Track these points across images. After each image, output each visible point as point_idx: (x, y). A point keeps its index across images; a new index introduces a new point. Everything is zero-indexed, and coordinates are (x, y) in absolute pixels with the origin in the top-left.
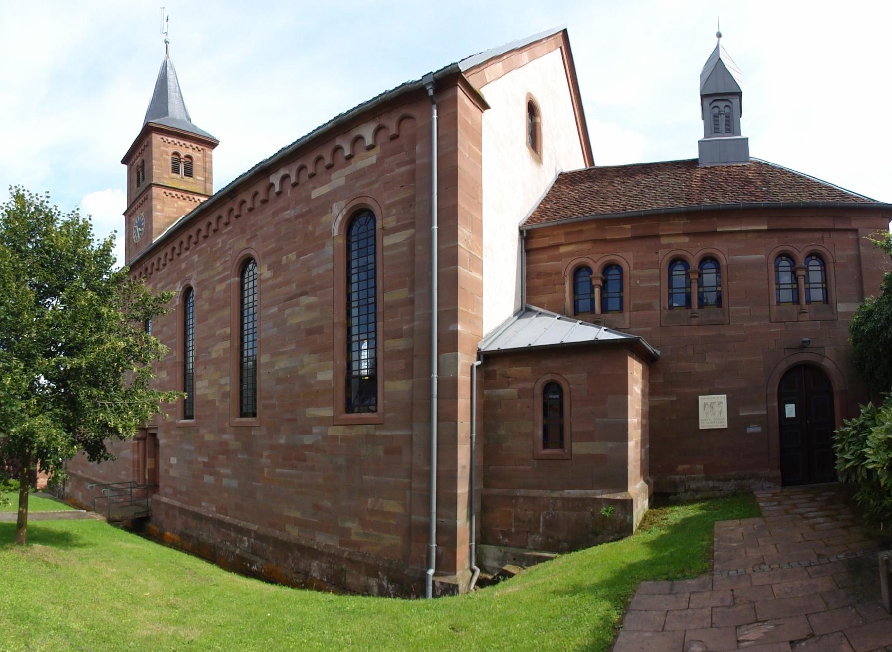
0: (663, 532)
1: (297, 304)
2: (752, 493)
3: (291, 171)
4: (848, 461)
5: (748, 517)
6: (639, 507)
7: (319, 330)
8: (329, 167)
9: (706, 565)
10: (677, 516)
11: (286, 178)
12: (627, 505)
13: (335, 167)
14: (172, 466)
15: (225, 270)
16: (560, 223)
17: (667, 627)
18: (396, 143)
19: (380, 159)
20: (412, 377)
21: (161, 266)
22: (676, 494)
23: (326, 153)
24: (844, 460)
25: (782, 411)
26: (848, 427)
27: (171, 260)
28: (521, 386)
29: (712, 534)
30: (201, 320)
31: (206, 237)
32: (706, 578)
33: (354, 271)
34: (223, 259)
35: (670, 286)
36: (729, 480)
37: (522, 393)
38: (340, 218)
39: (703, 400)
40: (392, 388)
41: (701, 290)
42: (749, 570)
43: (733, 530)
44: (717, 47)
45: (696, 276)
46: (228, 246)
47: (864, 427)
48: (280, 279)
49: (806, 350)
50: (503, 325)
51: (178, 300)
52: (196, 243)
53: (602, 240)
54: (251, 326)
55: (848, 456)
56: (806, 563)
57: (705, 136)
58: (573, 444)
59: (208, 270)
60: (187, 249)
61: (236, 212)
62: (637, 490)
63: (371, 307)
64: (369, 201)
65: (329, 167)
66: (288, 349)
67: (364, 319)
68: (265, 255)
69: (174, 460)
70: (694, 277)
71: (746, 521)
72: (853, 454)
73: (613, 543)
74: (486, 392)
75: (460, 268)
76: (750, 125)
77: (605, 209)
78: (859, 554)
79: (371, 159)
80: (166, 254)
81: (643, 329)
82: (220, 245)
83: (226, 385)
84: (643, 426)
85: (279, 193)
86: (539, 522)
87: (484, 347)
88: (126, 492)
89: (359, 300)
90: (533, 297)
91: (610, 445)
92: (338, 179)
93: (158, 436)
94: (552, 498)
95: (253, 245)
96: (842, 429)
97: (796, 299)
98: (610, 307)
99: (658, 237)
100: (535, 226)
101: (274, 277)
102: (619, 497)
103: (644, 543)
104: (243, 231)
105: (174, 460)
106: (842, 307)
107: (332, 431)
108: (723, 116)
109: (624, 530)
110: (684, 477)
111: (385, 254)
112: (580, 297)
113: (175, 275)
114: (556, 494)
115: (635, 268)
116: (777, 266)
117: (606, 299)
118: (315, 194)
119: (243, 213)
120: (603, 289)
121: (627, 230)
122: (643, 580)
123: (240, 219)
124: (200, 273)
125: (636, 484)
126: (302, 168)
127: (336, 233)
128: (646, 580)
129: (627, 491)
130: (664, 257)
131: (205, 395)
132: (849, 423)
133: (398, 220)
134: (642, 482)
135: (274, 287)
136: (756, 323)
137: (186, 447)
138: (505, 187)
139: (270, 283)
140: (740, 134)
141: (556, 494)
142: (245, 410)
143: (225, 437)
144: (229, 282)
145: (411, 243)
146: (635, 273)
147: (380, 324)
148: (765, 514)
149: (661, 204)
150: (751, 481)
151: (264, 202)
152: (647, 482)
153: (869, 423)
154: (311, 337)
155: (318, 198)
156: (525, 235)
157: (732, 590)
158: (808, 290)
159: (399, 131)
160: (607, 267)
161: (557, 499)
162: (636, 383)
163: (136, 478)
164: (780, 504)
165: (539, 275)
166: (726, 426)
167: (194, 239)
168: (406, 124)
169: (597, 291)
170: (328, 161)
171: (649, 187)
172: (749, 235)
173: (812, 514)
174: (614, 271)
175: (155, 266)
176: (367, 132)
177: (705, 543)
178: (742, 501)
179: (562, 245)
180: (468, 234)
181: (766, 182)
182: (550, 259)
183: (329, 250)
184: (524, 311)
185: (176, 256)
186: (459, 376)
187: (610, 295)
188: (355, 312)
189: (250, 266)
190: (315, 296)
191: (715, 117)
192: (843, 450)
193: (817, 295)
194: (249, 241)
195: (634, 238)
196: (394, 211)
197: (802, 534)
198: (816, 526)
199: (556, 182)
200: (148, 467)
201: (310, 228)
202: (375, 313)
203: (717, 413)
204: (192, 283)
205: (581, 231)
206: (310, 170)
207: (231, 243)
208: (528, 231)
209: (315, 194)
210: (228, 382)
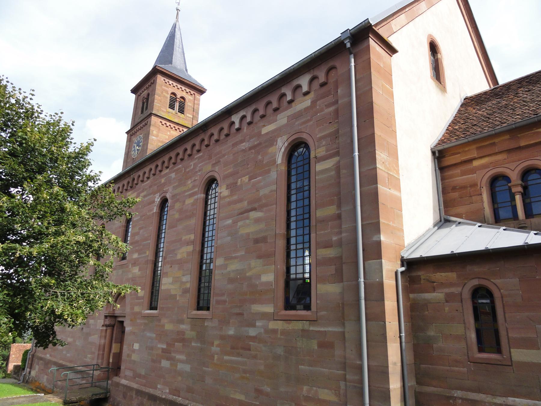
1: (248, 218)
3: (247, 112)
7: (264, 240)
8: (276, 110)
11: (244, 117)
13: (279, 110)
14: (134, 351)
15: (194, 187)
16: (470, 139)
18: (325, 88)
19: (314, 103)
20: (342, 282)
21: (145, 179)
23: (274, 99)
27: (154, 175)
28: (447, 290)
30: (172, 227)
31: (182, 160)
33: (293, 192)
34: (193, 179)
37: (449, 298)
38: (283, 150)
40: (325, 291)
46: (198, 169)
48: (235, 197)
50: (424, 235)
51: (155, 208)
52: (174, 164)
54: (210, 234)
59: (180, 186)
60: (167, 168)
61: (206, 142)
63: (306, 221)
64: (304, 136)
65: (276, 110)
66: (239, 254)
67: (300, 232)
68: (226, 177)
69: (136, 346)
74: (411, 296)
75: (379, 186)
77: (515, 119)
79: (307, 102)
80: (151, 170)
82: (192, 167)
83: (187, 282)
85: (238, 130)
87: (407, 255)
88: (89, 374)
89: (296, 216)
90: (451, 206)
92: (282, 119)
93: (125, 324)
95: (217, 169)
100: (446, 146)
101: (231, 195)
104: (210, 158)
105: (136, 346)
107: (272, 325)
111: (317, 178)
112: (500, 205)
113: (155, 187)
118: (264, 131)
119: (211, 144)
123: (209, 148)
124: (175, 188)
126: (256, 110)
127: (279, 161)
131: (169, 290)
133: (327, 150)
135: (230, 203)
137: (148, 334)
138: (415, 115)
139: (228, 200)
142: (201, 305)
143: (183, 327)
144: (196, 197)
145: (338, 168)
147: (313, 235)
151: (227, 135)
154: (257, 245)
155: (267, 134)
156: (437, 155)
159: (327, 79)
163: (100, 361)
165: (454, 189)
167: (173, 160)
168: (333, 73)
169: (518, 199)
170: (275, 105)
175: (141, 179)
176: (304, 81)
179: (475, 159)
180: (385, 157)
182: (464, 173)
183: (273, 175)
184: (443, 222)
185: (158, 172)
186: (384, 280)
188: (293, 225)
189: (214, 186)
190: (261, 211)
194: (214, 165)
196: (324, 143)
199: (462, 106)
200: (113, 351)
201: (260, 157)
202: (309, 226)
204: (168, 196)
205: (494, 144)
206: (261, 112)
207: (200, 167)
208: (440, 151)
209: (264, 131)
210: (189, 280)
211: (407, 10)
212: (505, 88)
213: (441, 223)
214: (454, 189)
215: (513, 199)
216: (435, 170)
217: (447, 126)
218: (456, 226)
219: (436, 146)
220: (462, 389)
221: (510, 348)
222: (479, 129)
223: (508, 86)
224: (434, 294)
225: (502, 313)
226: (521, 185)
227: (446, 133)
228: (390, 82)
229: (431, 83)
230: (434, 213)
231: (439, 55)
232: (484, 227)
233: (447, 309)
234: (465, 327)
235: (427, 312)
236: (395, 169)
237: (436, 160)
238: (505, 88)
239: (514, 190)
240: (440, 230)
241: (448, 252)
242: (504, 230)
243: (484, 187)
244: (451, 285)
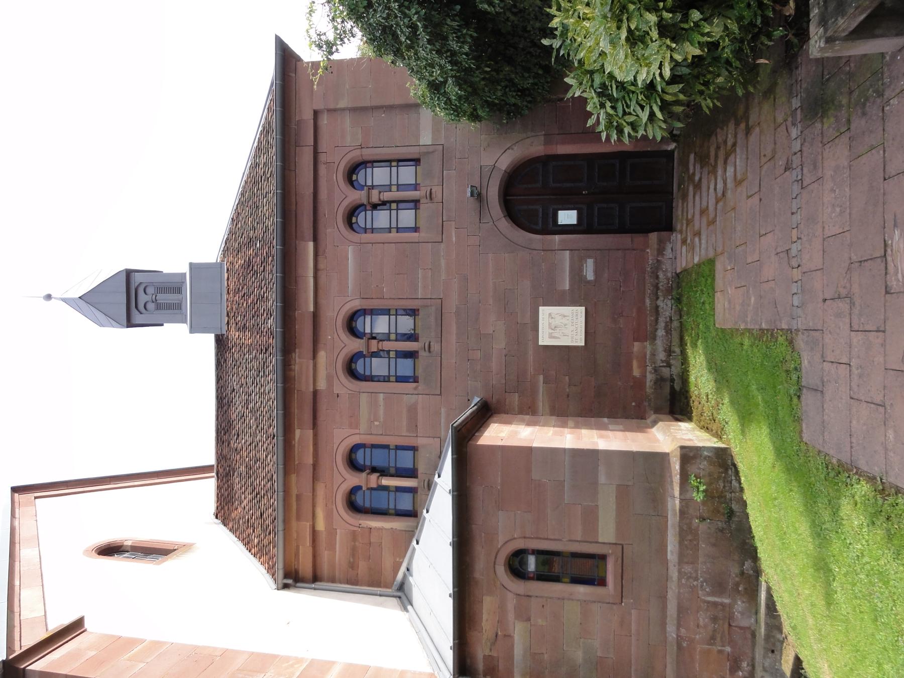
0: (726, 400)
2: (678, 275)
4: (652, 115)
5: (713, 279)
6: (690, 436)
9: (781, 339)
10: (704, 379)
12: (688, 455)
16: (281, 527)
17: (878, 399)
22: (672, 380)
24: (649, 126)
25: (567, 230)
26: (599, 115)
28: (511, 616)
29: (734, 332)
32: (801, 342)
35: (386, 379)
36: (657, 307)
37: (524, 615)
39: (544, 339)
41: (393, 337)
42: (796, 274)
43: (730, 302)
44: (65, 300)
45: (374, 342)
47: (603, 92)
49: (484, 192)
53: (314, 469)
55: (644, 116)
56: (796, 188)
57: (185, 322)
58: (600, 540)
62: (667, 437)
70: (374, 346)
71: (719, 283)
72: (642, 108)
73: (743, 479)
76: (172, 261)
77: (272, 462)
78: (796, 103)
81: (443, 420)
84: (577, 426)
86: (715, 604)
91: (602, 479)
94: (679, 579)
96: (602, 127)
97: (412, 205)
98: (410, 465)
99: (315, 393)
100: (280, 565)
102: (676, 466)
103: (743, 432)
106: (426, 139)
108: (159, 296)
109: (723, 461)
110: (649, 369)
114: (674, 573)
115: (357, 427)
116: (365, 230)
117: (397, 469)
120: (383, 472)
121: (302, 435)
122: (801, 437)
125: (657, 441)
128: (801, 432)
129: (667, 454)
130: (344, 385)
132: (594, 117)
134: (654, 430)
136: (443, 262)
140: (185, 274)
141: (674, 573)
146: (363, 427)
148: (711, 254)
149: (271, 386)
150: (661, 275)
152: (655, 423)
153: (598, 80)
157: (825, 300)
158: (399, 187)
160: (353, 464)
161: (680, 572)
162: (516, 433)
164: (698, 234)
165: (352, 566)
166: (583, 308)
169: (385, 481)
171: (247, 402)
172: (321, 266)
173: (720, 186)
174: (360, 456)
177: (747, 342)
178: (686, 288)
181: (250, 242)
182: (332, 547)
184: (402, 594)
187: (392, 464)
191: (159, 307)
192: (634, 126)
193: (407, 174)
195: (315, 425)
197: (749, 197)
198: (739, 177)
203: (564, 321)
205: (298, 497)
208: (286, 575)
211: (17, 583)
212: (223, 462)
213: (404, 598)
214: (352, 566)
215: (386, 488)
216: (315, 589)
217: (249, 554)
218: (412, 576)
219: (275, 579)
220: (663, 624)
221: (597, 542)
222: (270, 511)
223: (221, 457)
224: (517, 637)
225: (547, 542)
226: (368, 474)
227: (260, 558)
228: (131, 643)
229: (169, 564)
230: (385, 607)
231: (125, 543)
232: (419, 536)
233: (540, 622)
234: (569, 599)
235: (546, 656)
236: (292, 666)
237: (298, 585)
238: (223, 462)
239: (374, 485)
240: (414, 604)
241: (450, 602)
242: (427, 512)
243: (361, 522)
244: (502, 608)
